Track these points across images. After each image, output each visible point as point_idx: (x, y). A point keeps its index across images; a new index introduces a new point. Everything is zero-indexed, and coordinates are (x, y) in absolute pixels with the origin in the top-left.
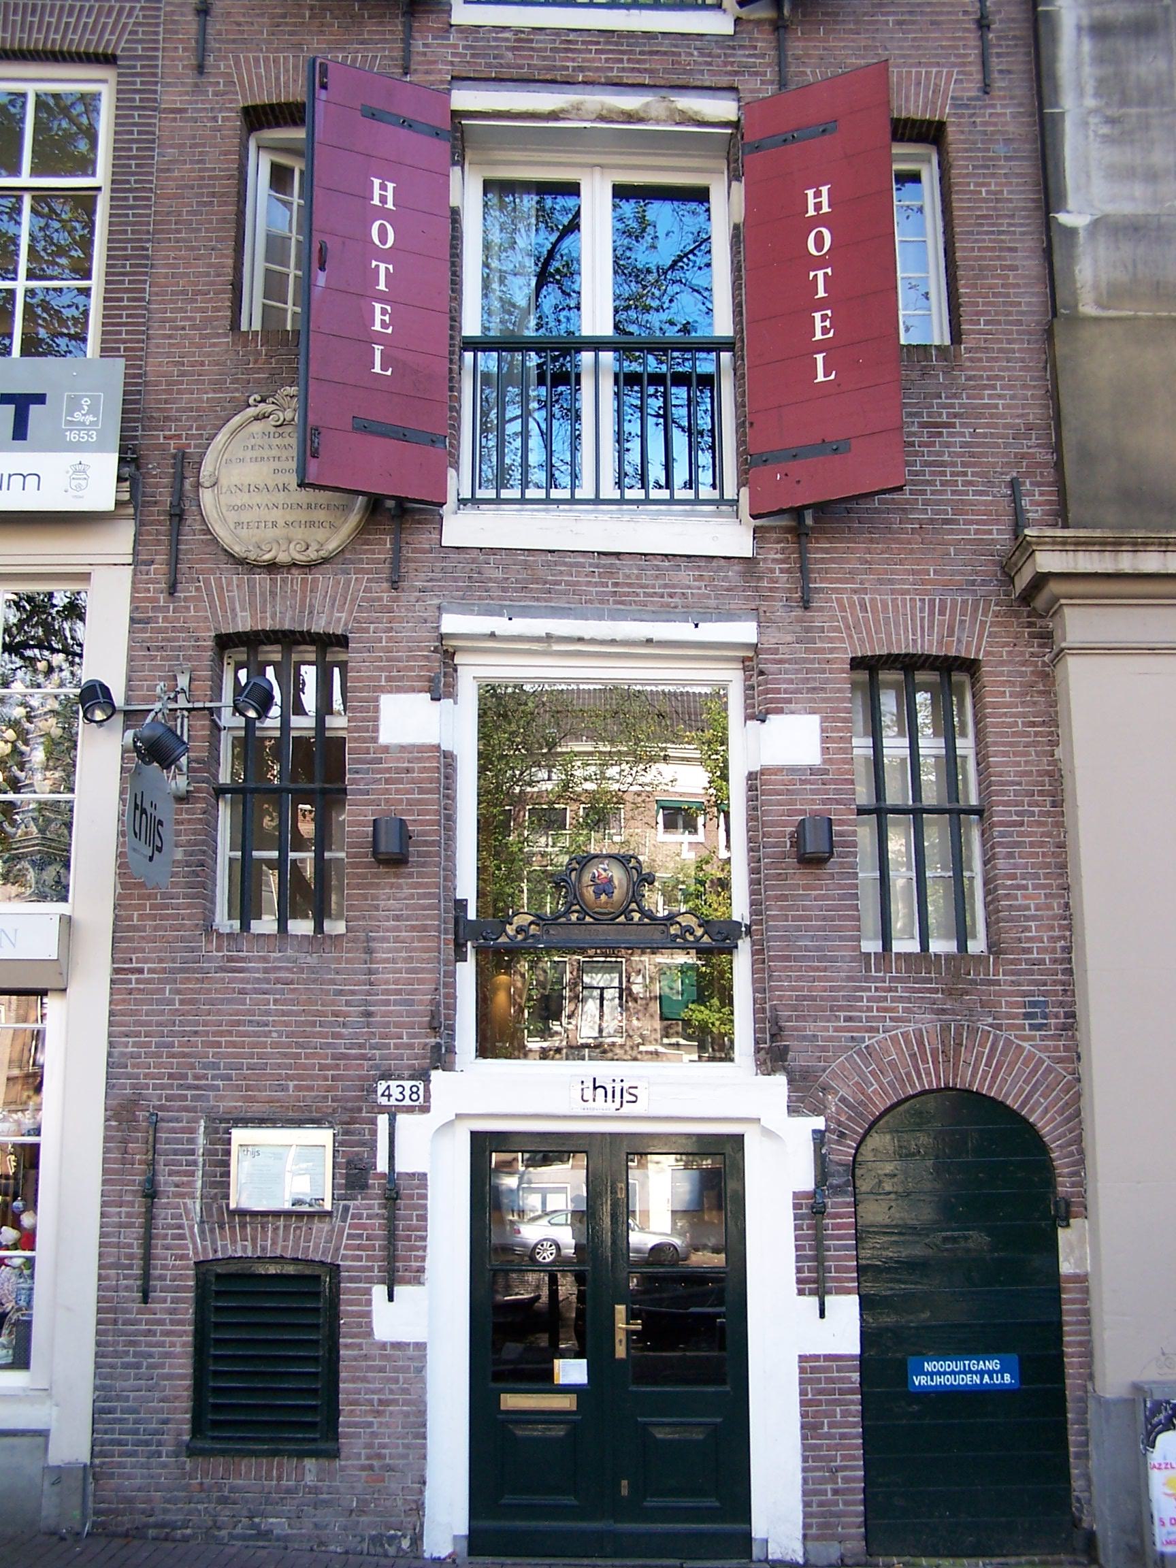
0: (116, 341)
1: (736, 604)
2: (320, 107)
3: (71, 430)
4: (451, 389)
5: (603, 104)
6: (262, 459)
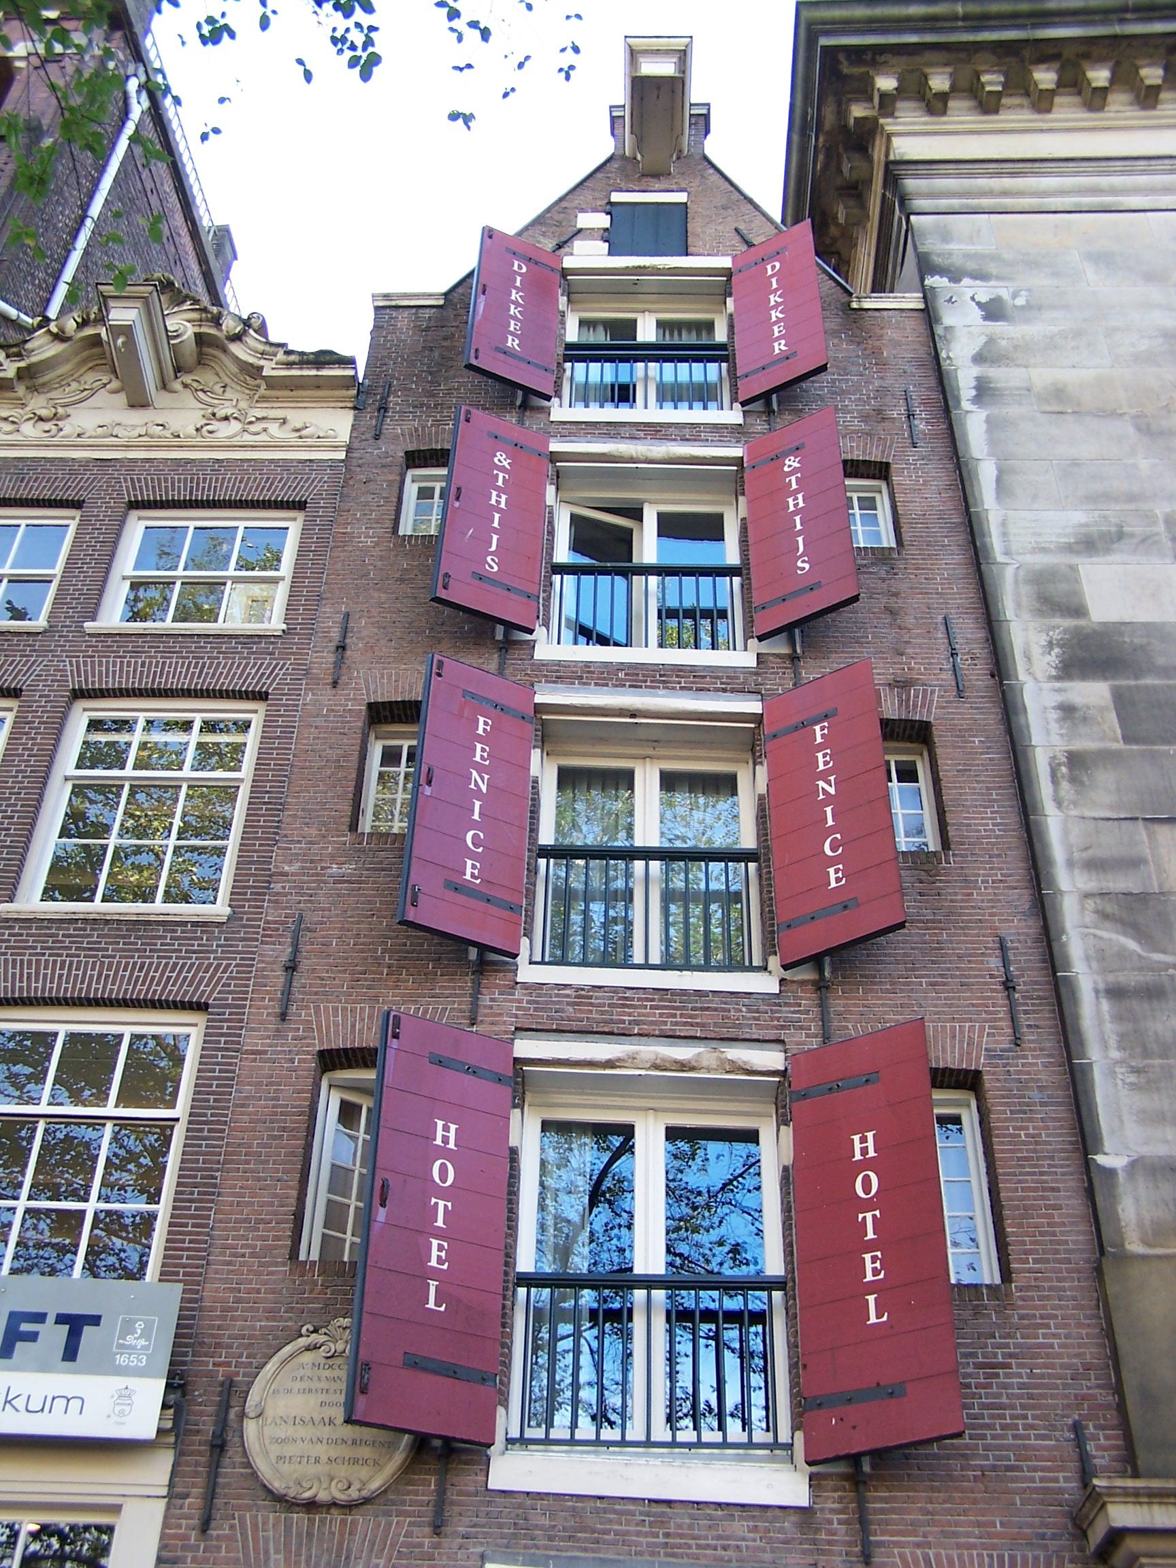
0: (176, 1266)
2: (390, 1054)
3: (122, 1354)
4: (504, 1325)
5: (657, 1054)
6: (310, 1391)
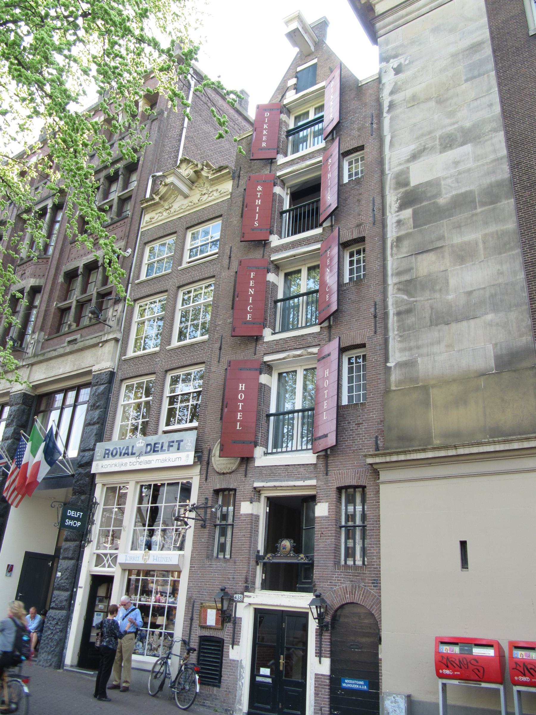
1: (312, 475)
